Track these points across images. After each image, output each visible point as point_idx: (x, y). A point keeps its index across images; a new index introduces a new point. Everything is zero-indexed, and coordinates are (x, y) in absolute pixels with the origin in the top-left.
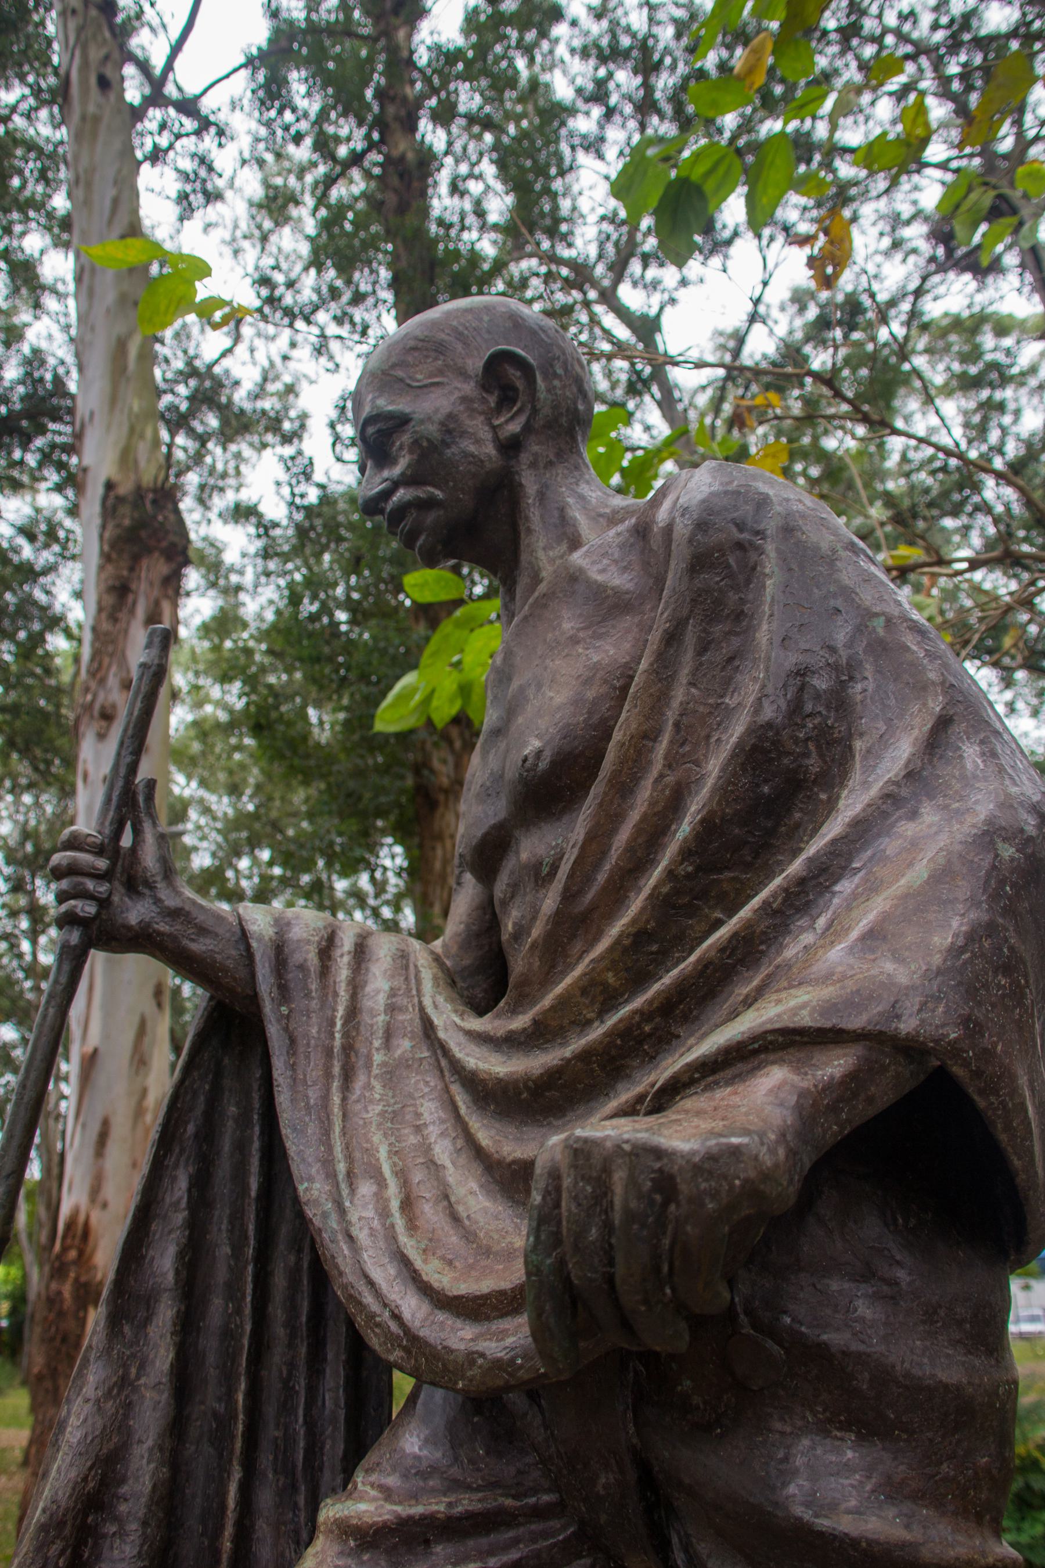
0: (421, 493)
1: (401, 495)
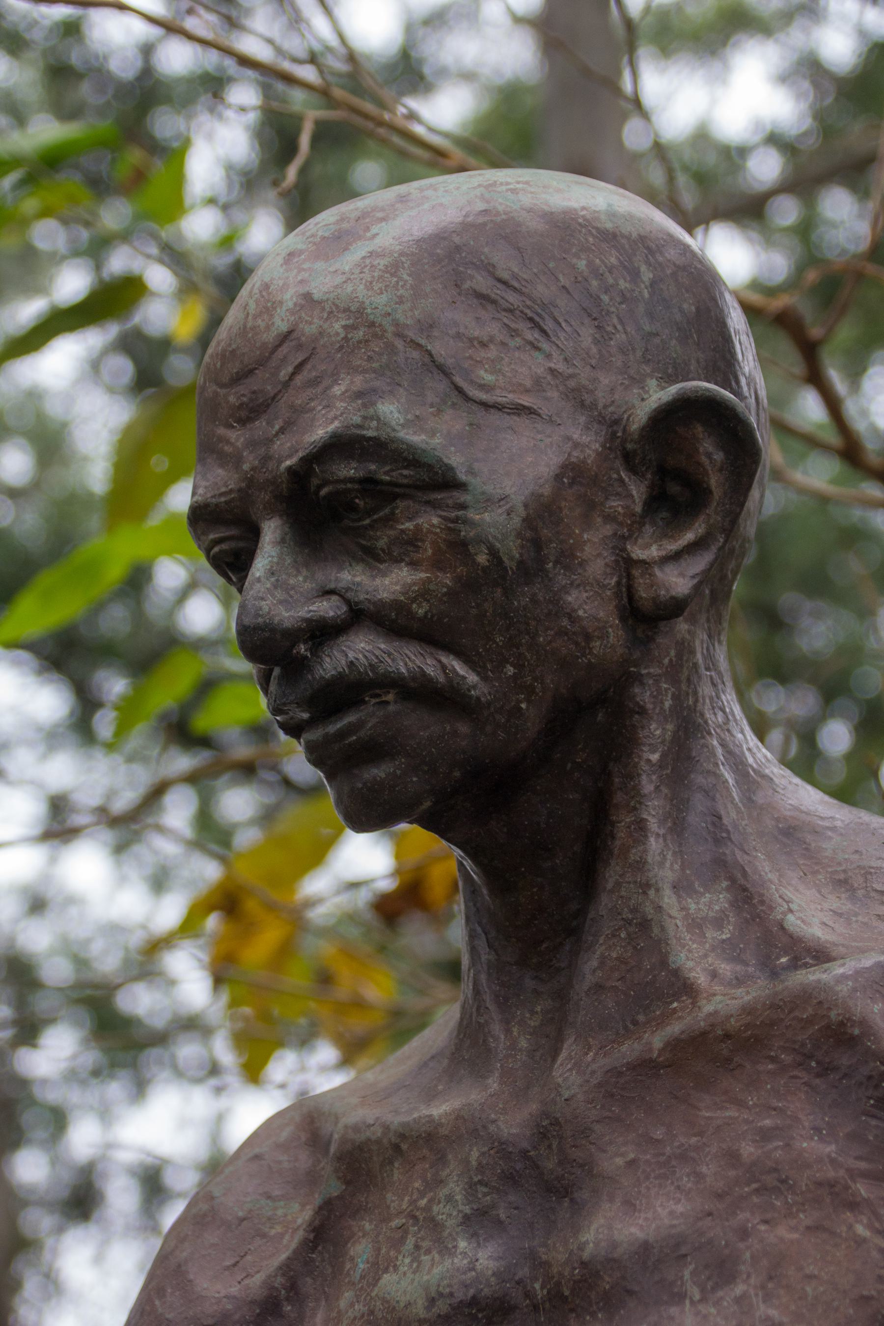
0: (409, 660)
1: (361, 649)
